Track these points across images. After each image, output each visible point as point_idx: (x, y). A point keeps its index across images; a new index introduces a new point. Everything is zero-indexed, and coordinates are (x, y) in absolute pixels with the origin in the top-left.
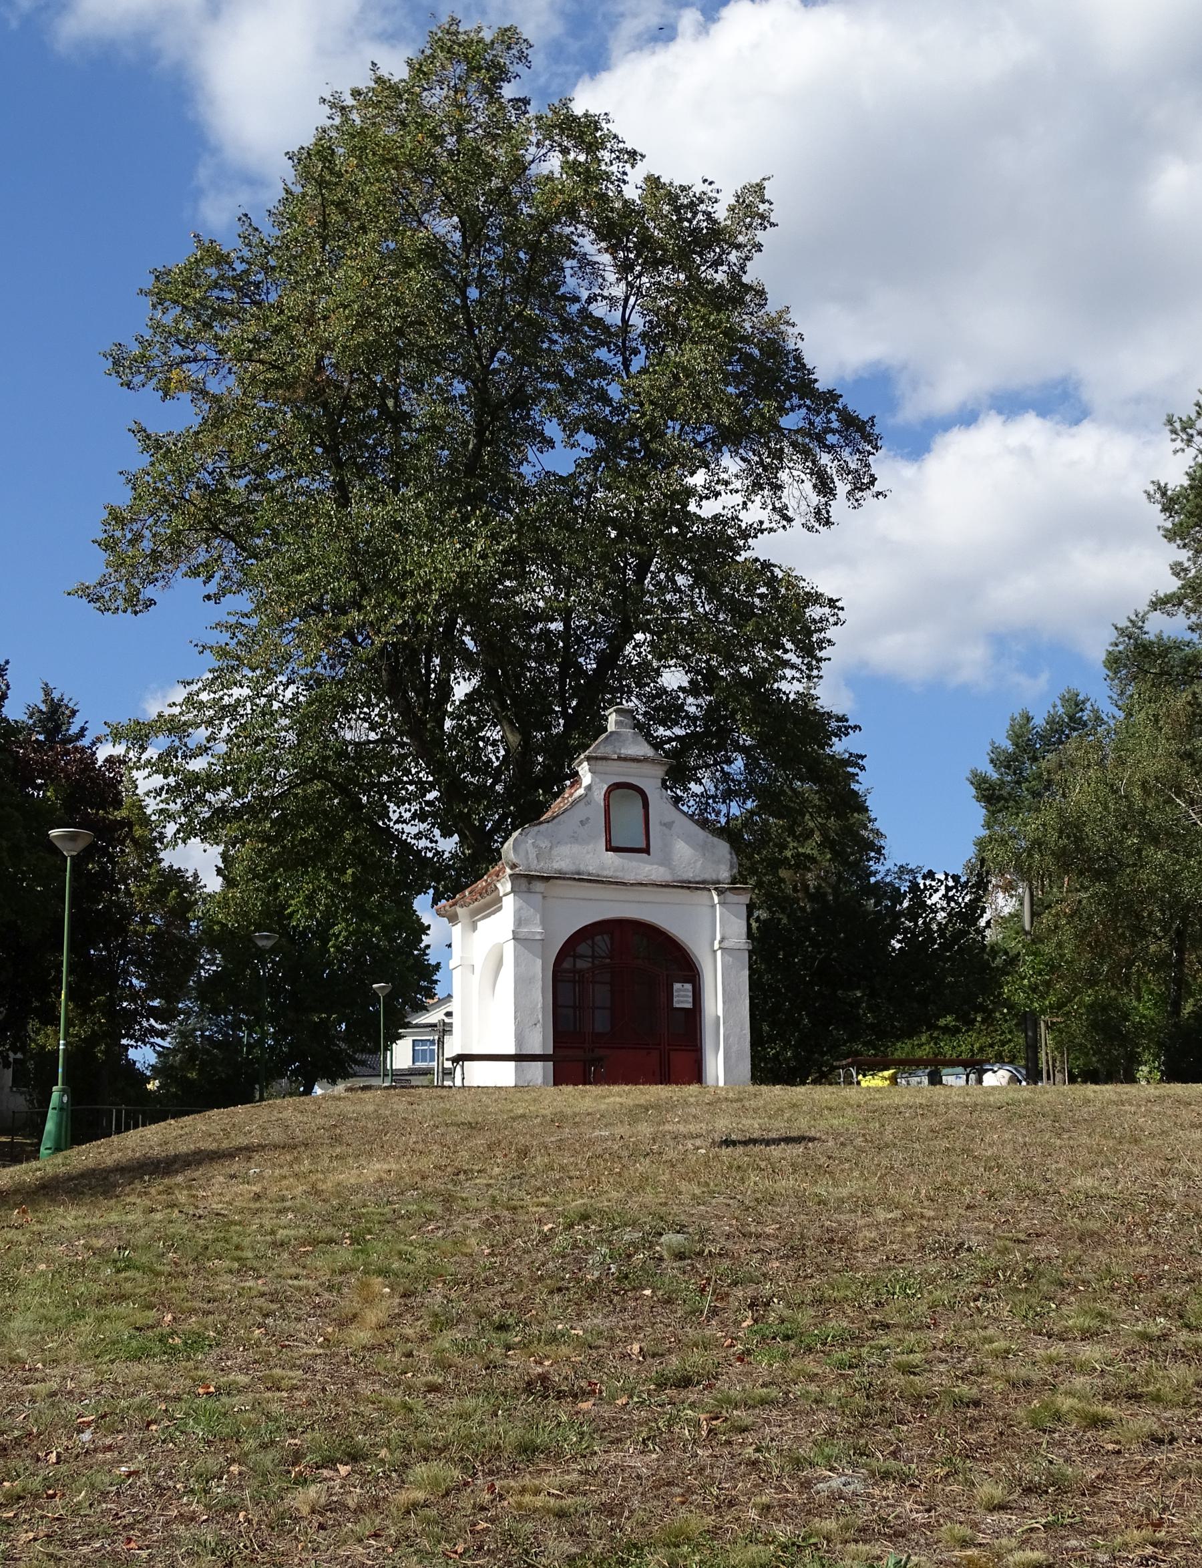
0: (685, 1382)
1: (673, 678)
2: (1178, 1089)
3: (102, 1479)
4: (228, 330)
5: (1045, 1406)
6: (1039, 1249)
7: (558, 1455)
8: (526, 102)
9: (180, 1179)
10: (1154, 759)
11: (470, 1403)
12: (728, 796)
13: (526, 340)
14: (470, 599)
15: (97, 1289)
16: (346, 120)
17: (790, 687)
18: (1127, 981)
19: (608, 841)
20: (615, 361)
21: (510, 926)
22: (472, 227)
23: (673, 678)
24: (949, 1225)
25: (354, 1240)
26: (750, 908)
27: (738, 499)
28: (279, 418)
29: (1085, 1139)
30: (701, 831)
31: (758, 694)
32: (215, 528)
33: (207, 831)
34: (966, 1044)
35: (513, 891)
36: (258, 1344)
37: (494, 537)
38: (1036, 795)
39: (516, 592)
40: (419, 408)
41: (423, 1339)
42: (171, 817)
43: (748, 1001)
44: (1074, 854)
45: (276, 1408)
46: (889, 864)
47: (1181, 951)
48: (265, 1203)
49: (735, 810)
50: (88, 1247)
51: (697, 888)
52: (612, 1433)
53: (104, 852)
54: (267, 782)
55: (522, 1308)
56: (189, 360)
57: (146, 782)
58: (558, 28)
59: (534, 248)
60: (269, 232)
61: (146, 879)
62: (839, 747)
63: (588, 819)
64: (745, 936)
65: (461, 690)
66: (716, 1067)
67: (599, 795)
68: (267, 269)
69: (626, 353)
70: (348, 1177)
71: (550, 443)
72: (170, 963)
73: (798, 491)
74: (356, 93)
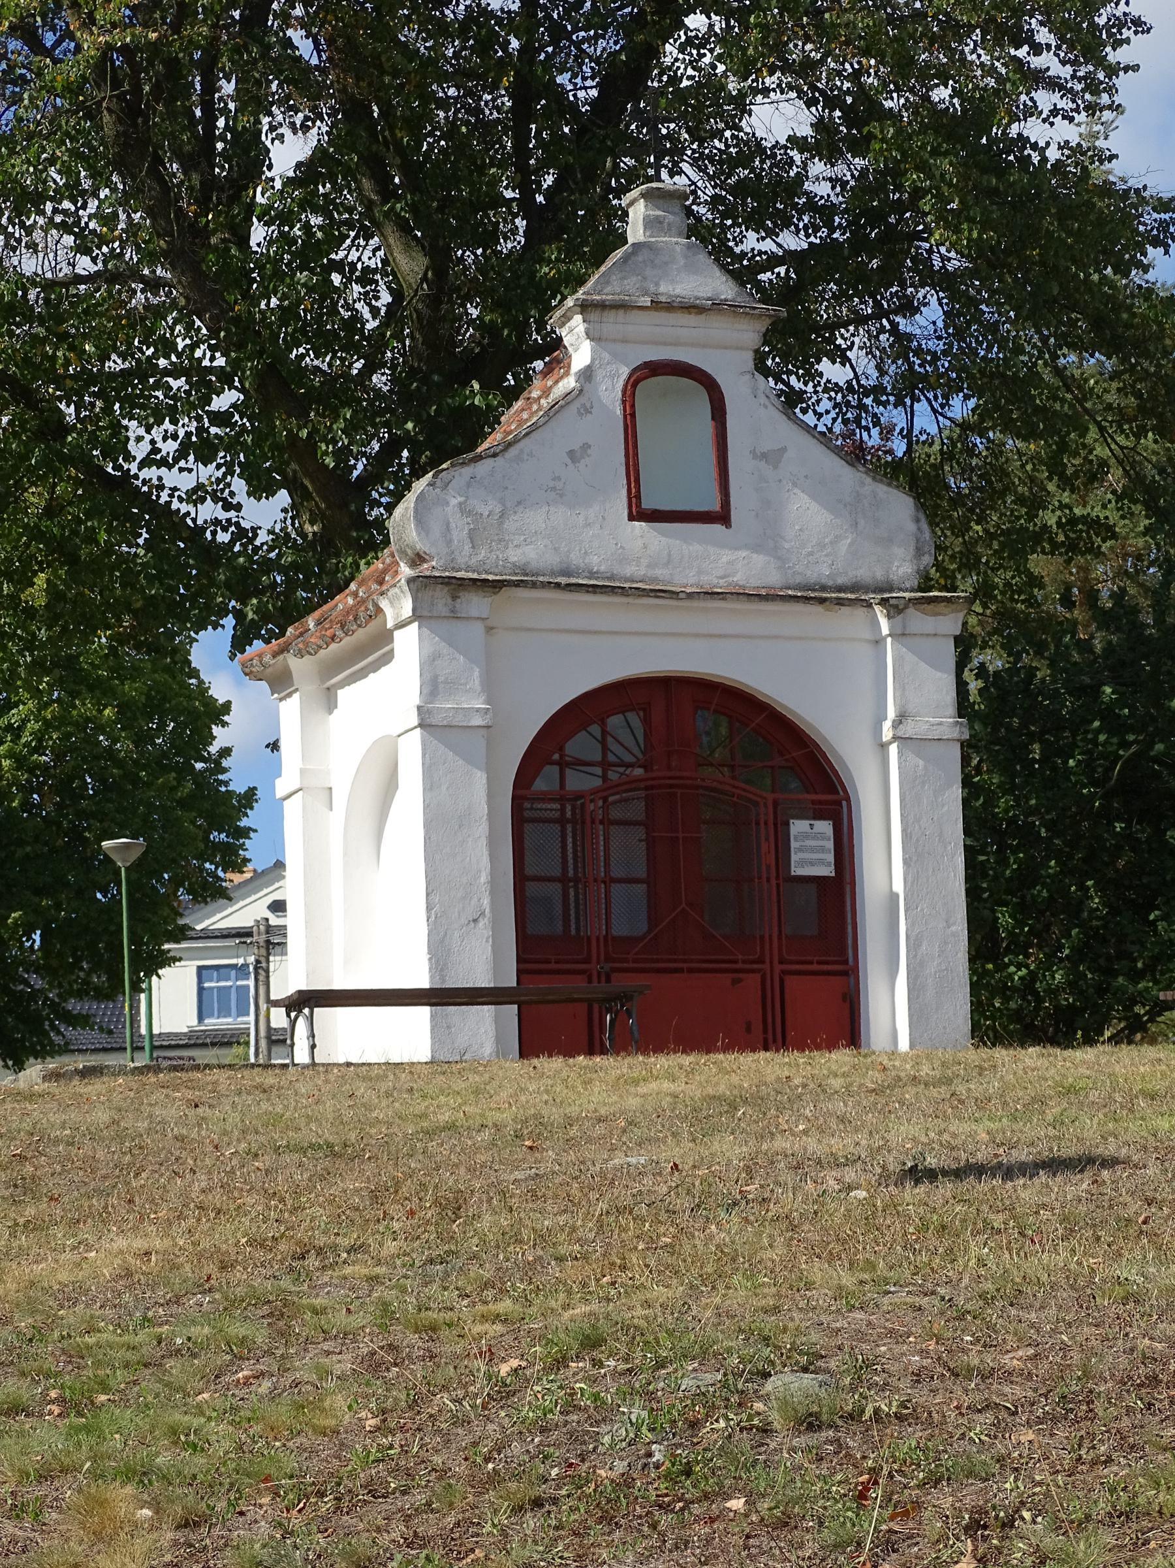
1: (778, 118)
12: (908, 388)
17: (1049, 134)
23: (778, 118)
26: (964, 644)
35: (417, 616)
51: (840, 602)
63: (586, 447)
65: (287, 153)
67: (610, 391)
70: (54, 1269)
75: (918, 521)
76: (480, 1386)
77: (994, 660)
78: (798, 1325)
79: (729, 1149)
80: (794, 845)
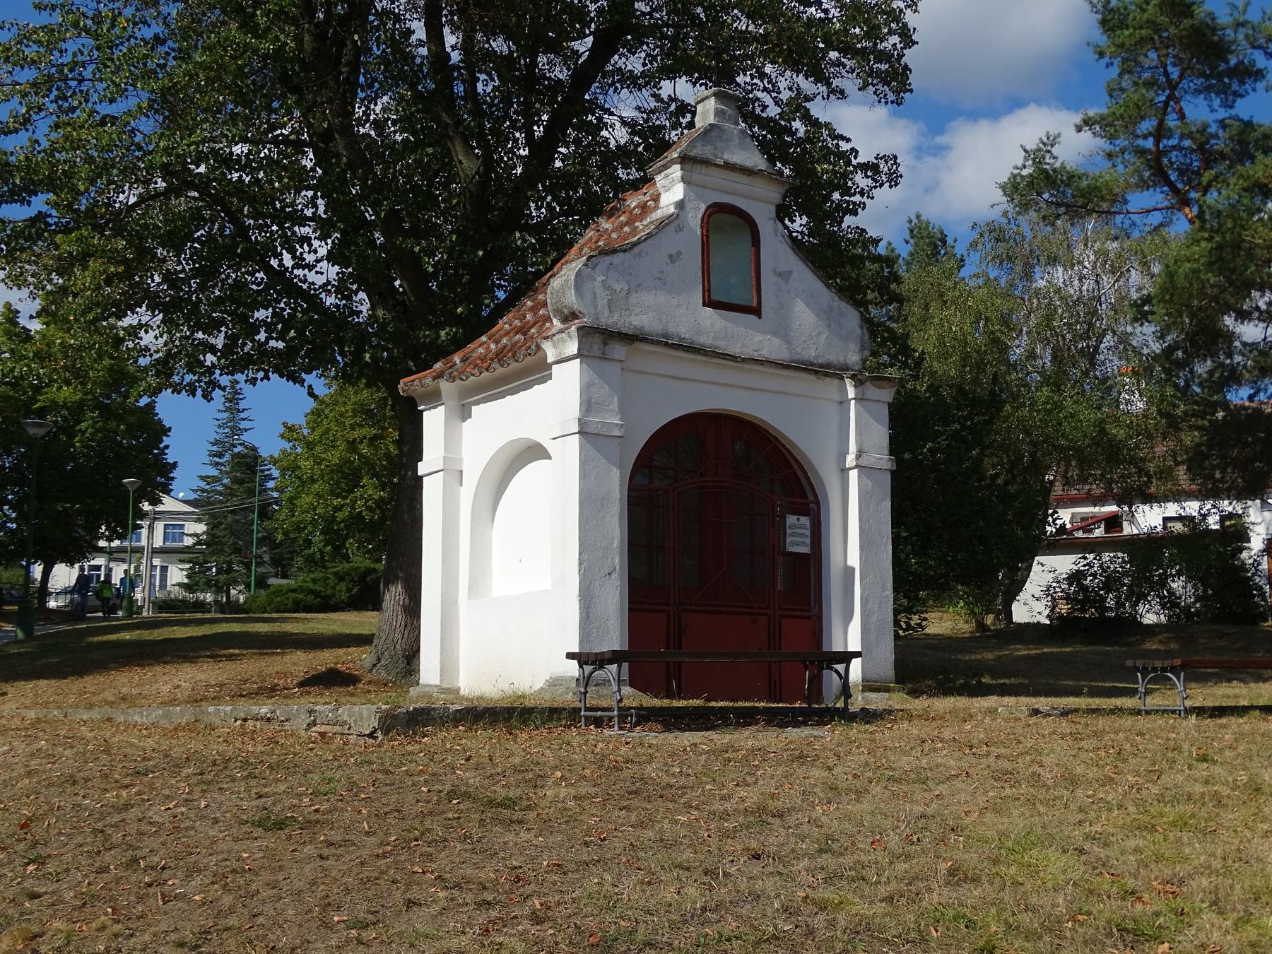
19: (707, 291)
30: (825, 291)
35: (579, 355)
43: (890, 547)
51: (827, 375)
63: (679, 253)
64: (886, 451)
75: (862, 328)
80: (788, 531)
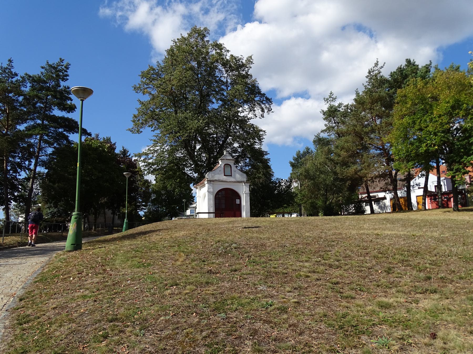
0: (236, 271)
1: (236, 145)
2: (325, 217)
3: (131, 289)
4: (155, 82)
5: (298, 274)
6: (299, 246)
7: (213, 284)
8: (209, 41)
9: (147, 235)
10: (322, 159)
11: (197, 275)
12: (246, 166)
13: (209, 84)
14: (199, 131)
15: (132, 255)
16: (176, 44)
17: (257, 146)
18: (317, 198)
20: (225, 88)
21: (207, 189)
22: (199, 64)
23: (236, 145)
24: (283, 242)
25: (178, 246)
26: (250, 186)
27: (247, 113)
28: (164, 98)
29: (308, 226)
31: (251, 148)
32: (153, 118)
33: (152, 173)
34: (288, 210)
36: (160, 265)
37: (204, 120)
38: (301, 165)
39: (207, 130)
40: (190, 96)
41: (190, 264)
42: (146, 170)
44: (307, 176)
45: (163, 276)
46: (275, 178)
47: (326, 193)
48: (162, 240)
49: (247, 168)
50: (130, 248)
52: (222, 280)
53: (134, 176)
54: (163, 164)
55: (208, 258)
56: (148, 88)
57: (141, 164)
58: (216, 27)
59: (210, 67)
60: (162, 65)
61: (141, 181)
62: (266, 157)
65: (198, 147)
66: (244, 214)
67: (223, 166)
68: (162, 71)
69: (227, 87)
70: (177, 235)
71: (214, 103)
72: (146, 196)
73: (258, 111)
74: (178, 39)
76: (210, 245)
77: (252, 187)
78: (235, 240)
79: (231, 225)
